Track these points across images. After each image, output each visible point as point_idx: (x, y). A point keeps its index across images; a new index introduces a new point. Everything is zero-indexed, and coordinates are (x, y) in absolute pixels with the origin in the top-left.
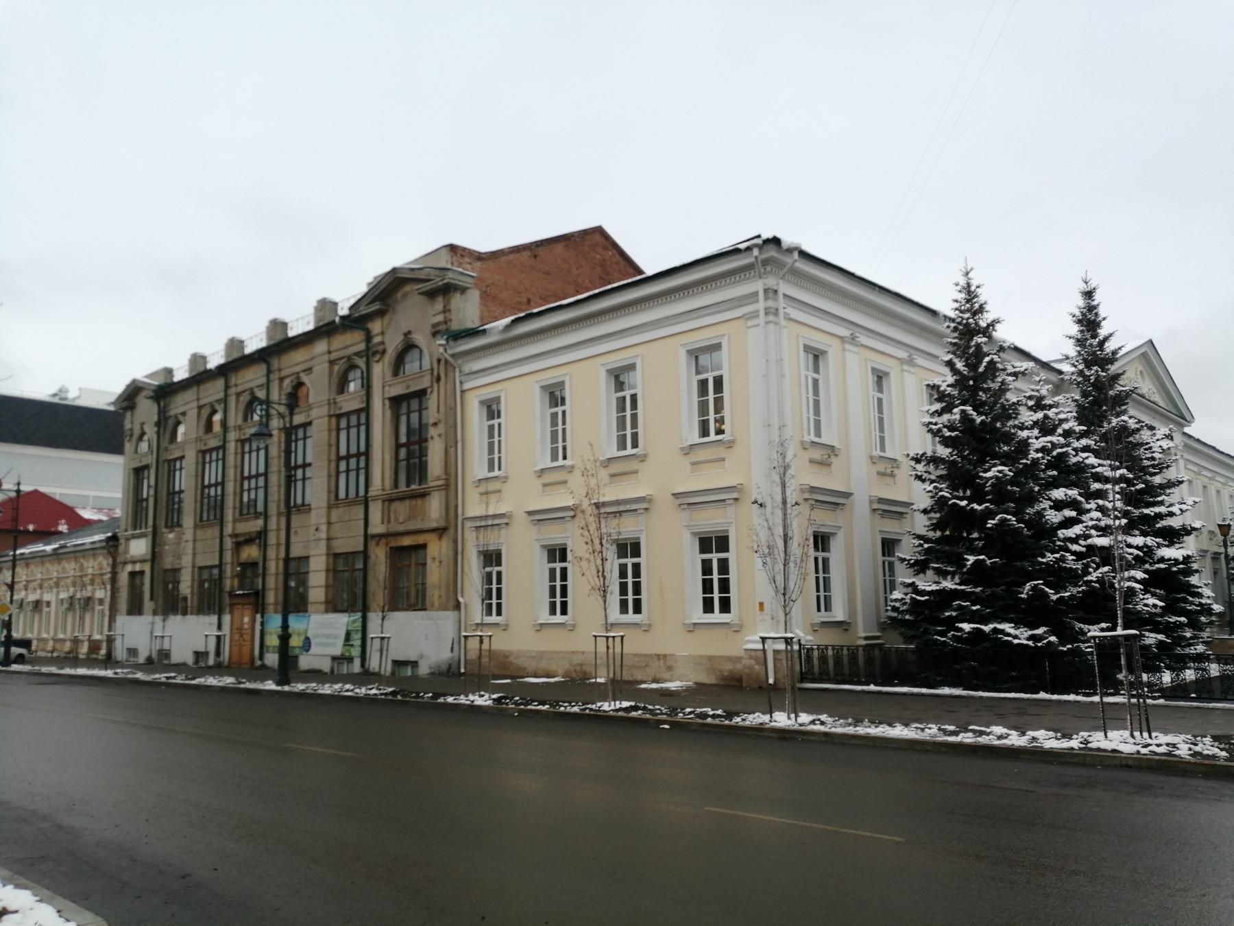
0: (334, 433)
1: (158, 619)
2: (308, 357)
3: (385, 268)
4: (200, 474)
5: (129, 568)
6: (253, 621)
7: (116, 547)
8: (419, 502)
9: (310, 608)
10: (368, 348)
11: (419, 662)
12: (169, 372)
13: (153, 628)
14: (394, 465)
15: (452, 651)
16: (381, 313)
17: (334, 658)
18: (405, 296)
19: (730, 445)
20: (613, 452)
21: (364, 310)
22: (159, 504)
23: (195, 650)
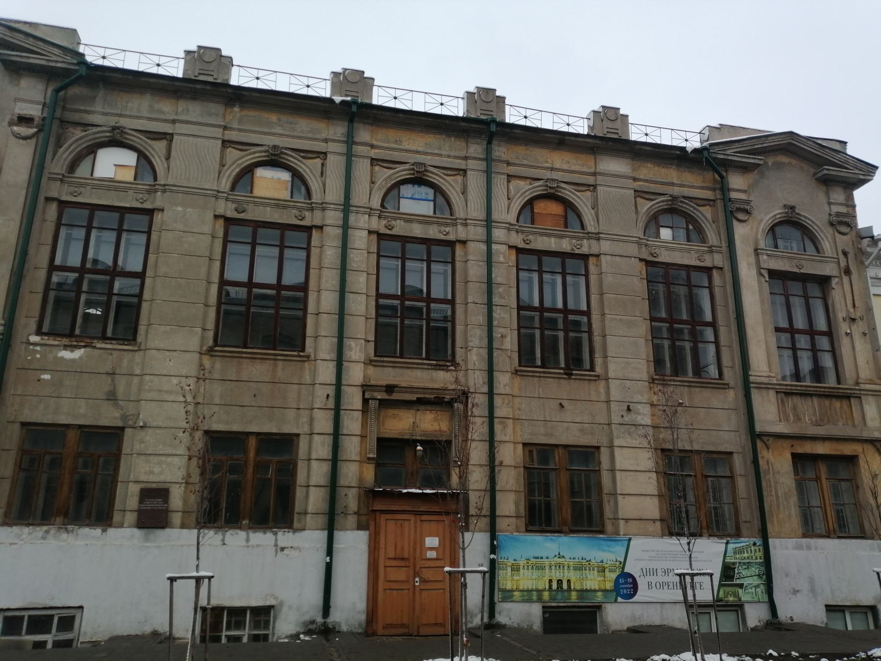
21: (731, 154)
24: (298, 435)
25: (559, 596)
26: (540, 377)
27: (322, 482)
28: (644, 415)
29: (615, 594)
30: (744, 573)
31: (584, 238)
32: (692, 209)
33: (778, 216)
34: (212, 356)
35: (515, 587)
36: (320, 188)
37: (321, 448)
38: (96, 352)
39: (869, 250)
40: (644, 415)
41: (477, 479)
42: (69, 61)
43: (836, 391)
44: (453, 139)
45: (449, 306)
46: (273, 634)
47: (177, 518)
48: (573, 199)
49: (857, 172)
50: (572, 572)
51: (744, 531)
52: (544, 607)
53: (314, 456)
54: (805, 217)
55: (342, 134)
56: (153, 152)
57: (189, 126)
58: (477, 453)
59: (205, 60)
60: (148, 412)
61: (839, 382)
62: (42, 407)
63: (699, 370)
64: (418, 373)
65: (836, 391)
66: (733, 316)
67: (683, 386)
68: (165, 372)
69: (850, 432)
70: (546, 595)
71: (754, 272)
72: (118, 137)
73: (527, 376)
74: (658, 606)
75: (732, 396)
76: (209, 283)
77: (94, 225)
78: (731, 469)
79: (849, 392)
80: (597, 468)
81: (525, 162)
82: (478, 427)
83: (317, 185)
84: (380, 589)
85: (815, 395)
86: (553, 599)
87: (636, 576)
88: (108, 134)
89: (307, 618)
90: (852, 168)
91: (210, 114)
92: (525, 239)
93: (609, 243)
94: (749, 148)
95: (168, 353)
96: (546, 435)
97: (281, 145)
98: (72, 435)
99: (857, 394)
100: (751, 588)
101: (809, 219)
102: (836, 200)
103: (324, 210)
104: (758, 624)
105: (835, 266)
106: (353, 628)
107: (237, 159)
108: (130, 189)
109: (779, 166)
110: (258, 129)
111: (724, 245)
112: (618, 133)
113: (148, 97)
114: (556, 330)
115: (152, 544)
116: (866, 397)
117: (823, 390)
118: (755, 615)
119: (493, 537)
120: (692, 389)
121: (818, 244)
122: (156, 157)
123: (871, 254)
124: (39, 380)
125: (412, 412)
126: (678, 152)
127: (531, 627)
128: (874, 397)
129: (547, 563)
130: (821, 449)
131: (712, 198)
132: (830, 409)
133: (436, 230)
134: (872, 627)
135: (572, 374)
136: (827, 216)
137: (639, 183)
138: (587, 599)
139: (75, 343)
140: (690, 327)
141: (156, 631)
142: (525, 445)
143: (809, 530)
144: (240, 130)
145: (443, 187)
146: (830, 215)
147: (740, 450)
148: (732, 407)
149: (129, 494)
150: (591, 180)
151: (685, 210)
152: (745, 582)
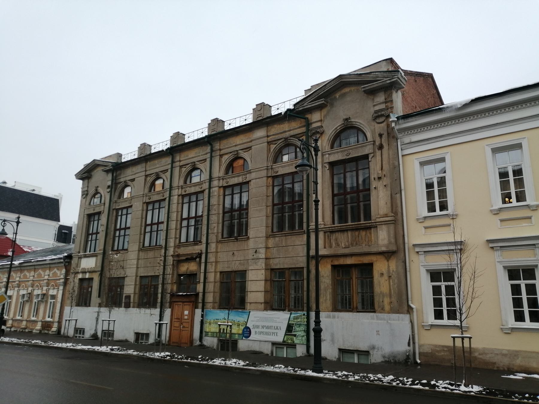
0: (180, 205)
1: (104, 311)
2: (249, 140)
3: (89, 161)
4: (144, 217)
5: (80, 276)
6: (192, 315)
7: (70, 263)
8: (363, 233)
9: (248, 306)
10: (308, 130)
12: (119, 155)
13: (98, 315)
14: (331, 208)
15: (409, 345)
16: (320, 108)
17: (274, 344)
18: (343, 95)
19: (454, 217)
20: (500, 205)
21: (307, 105)
22: (108, 237)
23: (136, 331)
26: (227, 242)
28: (262, 253)
30: (297, 329)
33: (338, 128)
40: (262, 253)
43: (359, 226)
49: (385, 79)
54: (355, 122)
65: (359, 226)
67: (282, 236)
69: (366, 249)
74: (259, 342)
76: (219, 214)
77: (334, 174)
79: (368, 225)
81: (227, 146)
84: (172, 330)
85: (350, 230)
87: (251, 328)
90: (382, 79)
93: (254, 173)
94: (316, 96)
97: (158, 171)
99: (374, 225)
100: (300, 337)
101: (357, 122)
102: (378, 102)
104: (302, 355)
108: (128, 200)
110: (153, 168)
112: (261, 116)
116: (381, 226)
117: (351, 226)
120: (287, 237)
127: (213, 347)
128: (386, 226)
130: (349, 261)
132: (358, 237)
135: (238, 239)
137: (270, 137)
143: (335, 309)
152: (297, 333)
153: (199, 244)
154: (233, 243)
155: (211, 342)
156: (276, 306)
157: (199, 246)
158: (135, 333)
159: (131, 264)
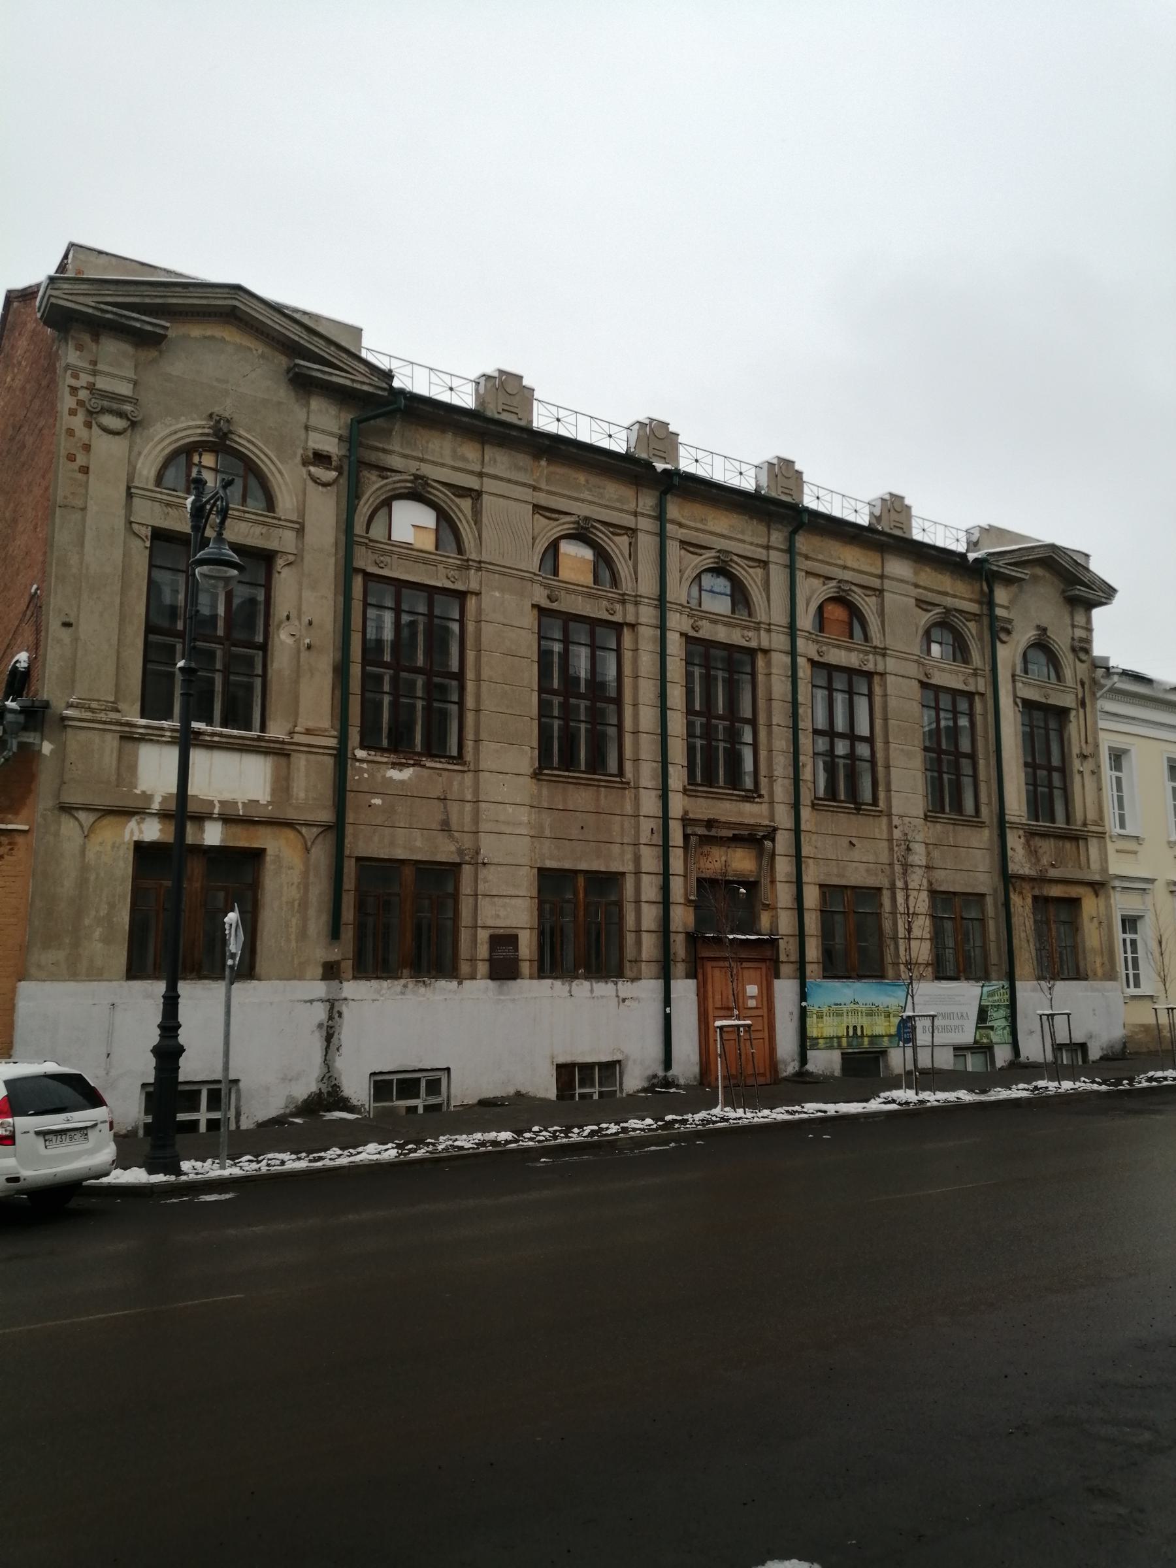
11: (1089, 1045)
21: (1001, 566)
23: (561, 1060)
24: (623, 874)
25: (855, 1043)
26: (833, 811)
27: (653, 927)
29: (897, 1038)
30: (995, 1015)
31: (870, 652)
32: (961, 624)
34: (539, 780)
35: (820, 1035)
36: (631, 575)
37: (650, 889)
38: (426, 772)
39: (1103, 681)
41: (786, 923)
42: (377, 384)
44: (755, 523)
45: (260, 653)
46: (621, 1090)
47: (525, 968)
48: (861, 604)
49: (1101, 594)
50: (864, 1017)
51: (994, 975)
52: (842, 1054)
53: (644, 898)
54: (1054, 641)
55: (651, 507)
56: (460, 515)
57: (499, 482)
58: (784, 895)
59: (507, 390)
60: (489, 848)
61: (1068, 823)
62: (376, 839)
63: (958, 807)
64: (727, 805)
66: (992, 748)
68: (500, 799)
70: (844, 1042)
71: (1011, 700)
72: (420, 489)
73: (823, 810)
75: (984, 837)
78: (983, 911)
80: (879, 911)
81: (821, 557)
82: (783, 867)
83: (627, 572)
86: (850, 1045)
88: (409, 485)
89: (650, 1072)
91: (519, 469)
92: (820, 650)
95: (501, 776)
96: (838, 876)
98: (408, 873)
103: (636, 604)
104: (1004, 1064)
105: (1074, 696)
106: (689, 1081)
107: (550, 530)
109: (1035, 579)
111: (988, 668)
113: (449, 436)
114: (412, 697)
115: (508, 997)
118: (1002, 1055)
119: (803, 985)
120: (956, 827)
121: (1060, 670)
122: (464, 521)
123: (1103, 686)
124: (370, 806)
125: (724, 849)
126: (958, 559)
129: (845, 1009)
131: (978, 612)
133: (740, 635)
134: (1080, 1063)
135: (860, 809)
136: (1070, 640)
138: (877, 1044)
139: (404, 761)
140: (392, 672)
141: (519, 1092)
142: (821, 886)
144: (550, 493)
145: (745, 582)
146: (1073, 639)
147: (991, 892)
148: (986, 847)
149: (479, 941)
150: (876, 583)
151: (954, 624)
152: (995, 1024)
153: (757, 800)
154: (847, 815)
155: (825, 1061)
156: (950, 970)
157: (755, 805)
158: (560, 1067)
159: (502, 818)
